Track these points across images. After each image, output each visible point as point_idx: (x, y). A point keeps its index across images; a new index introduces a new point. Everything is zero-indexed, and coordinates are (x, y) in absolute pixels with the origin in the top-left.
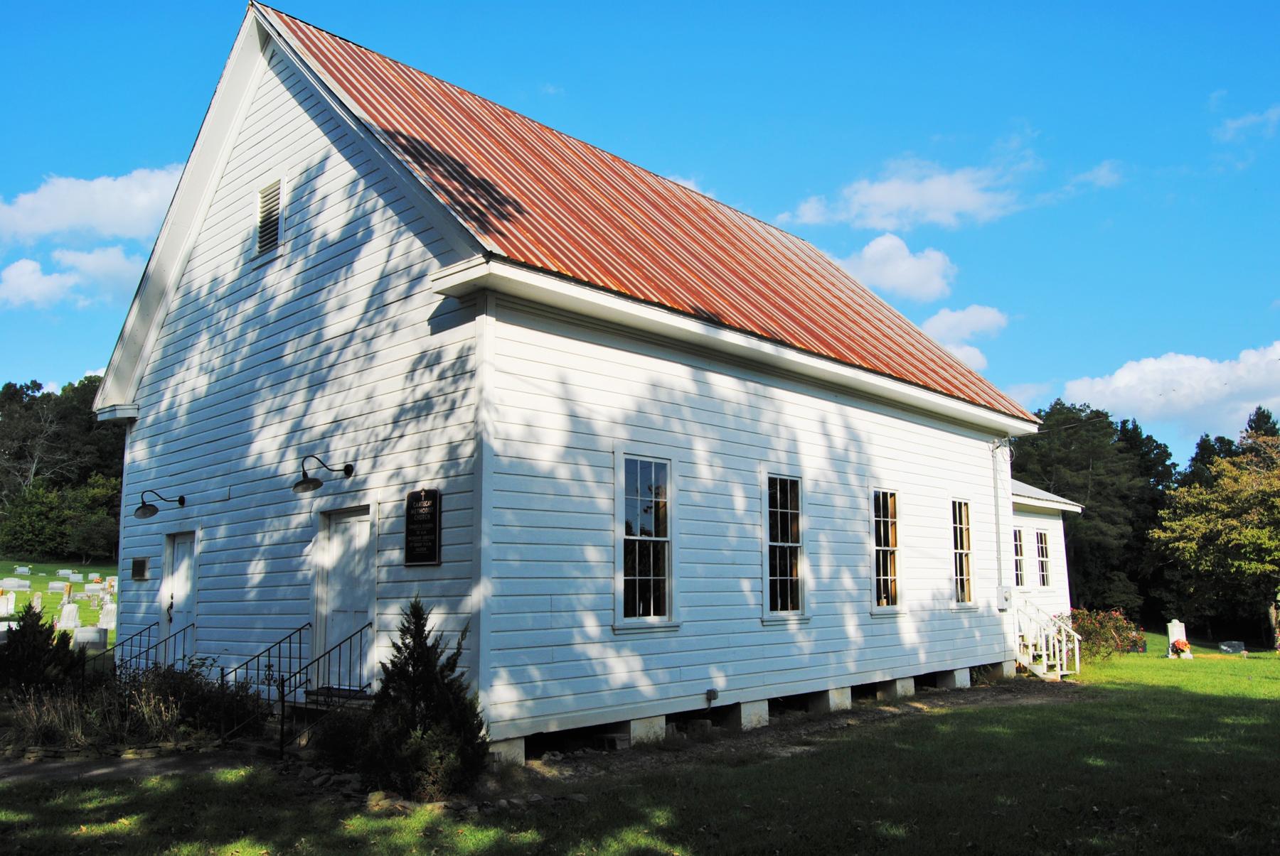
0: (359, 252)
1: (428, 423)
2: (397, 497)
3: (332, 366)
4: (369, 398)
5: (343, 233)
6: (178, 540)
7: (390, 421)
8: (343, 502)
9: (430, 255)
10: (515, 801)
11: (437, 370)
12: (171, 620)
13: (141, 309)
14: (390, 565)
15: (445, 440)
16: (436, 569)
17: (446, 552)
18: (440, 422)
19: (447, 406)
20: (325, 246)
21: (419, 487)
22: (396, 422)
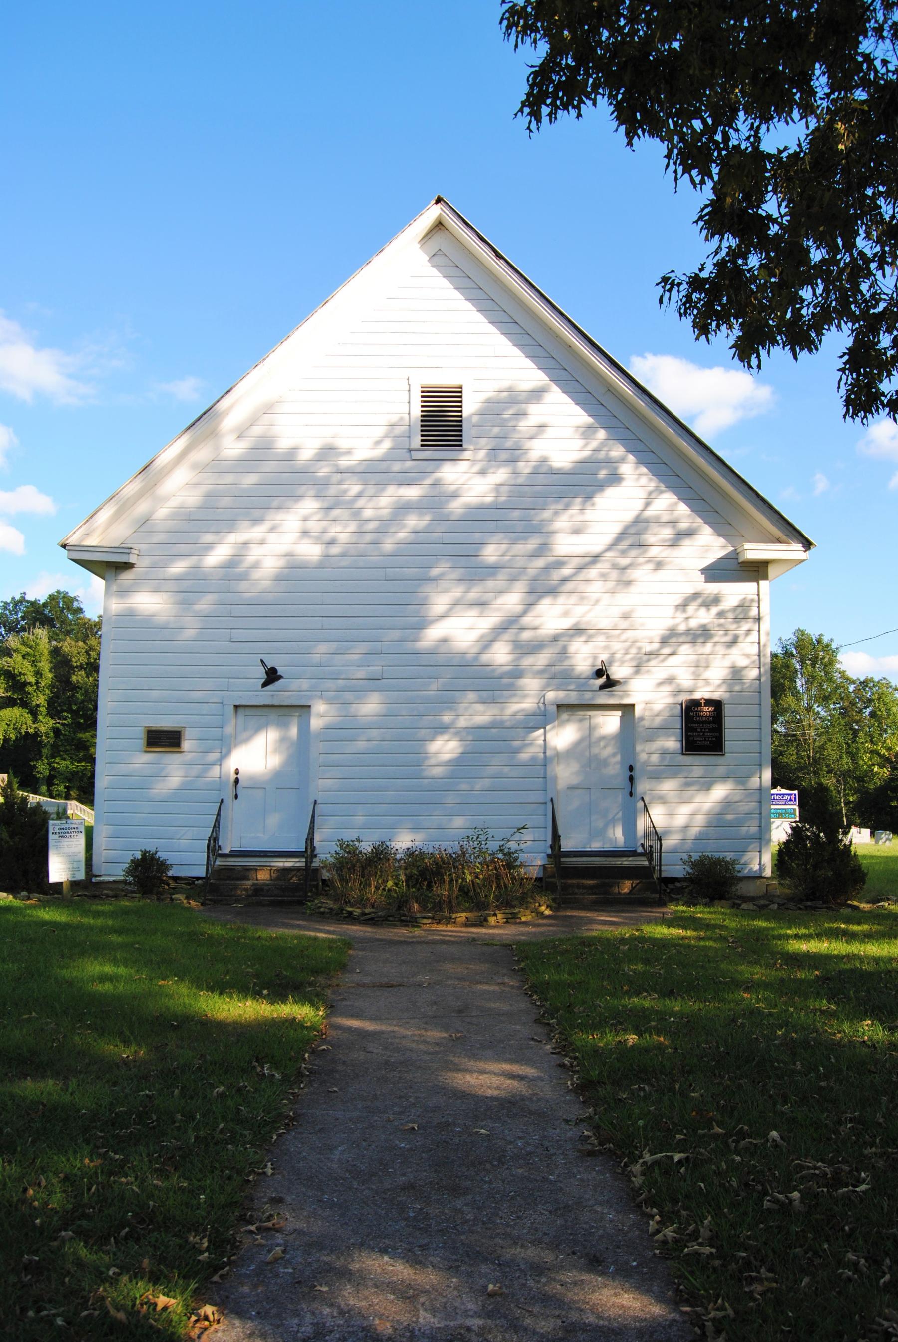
0: (602, 490)
1: (709, 647)
2: (670, 700)
3: (565, 580)
4: (626, 616)
5: (573, 468)
6: (240, 710)
7: (657, 639)
8: (593, 698)
9: (699, 520)
10: (206, 1244)
11: (714, 610)
12: (236, 797)
13: (536, 119)
14: (664, 752)
15: (727, 662)
16: (719, 757)
17: (728, 745)
18: (721, 649)
19: (728, 639)
20: (543, 468)
21: (697, 696)
22: (664, 641)
